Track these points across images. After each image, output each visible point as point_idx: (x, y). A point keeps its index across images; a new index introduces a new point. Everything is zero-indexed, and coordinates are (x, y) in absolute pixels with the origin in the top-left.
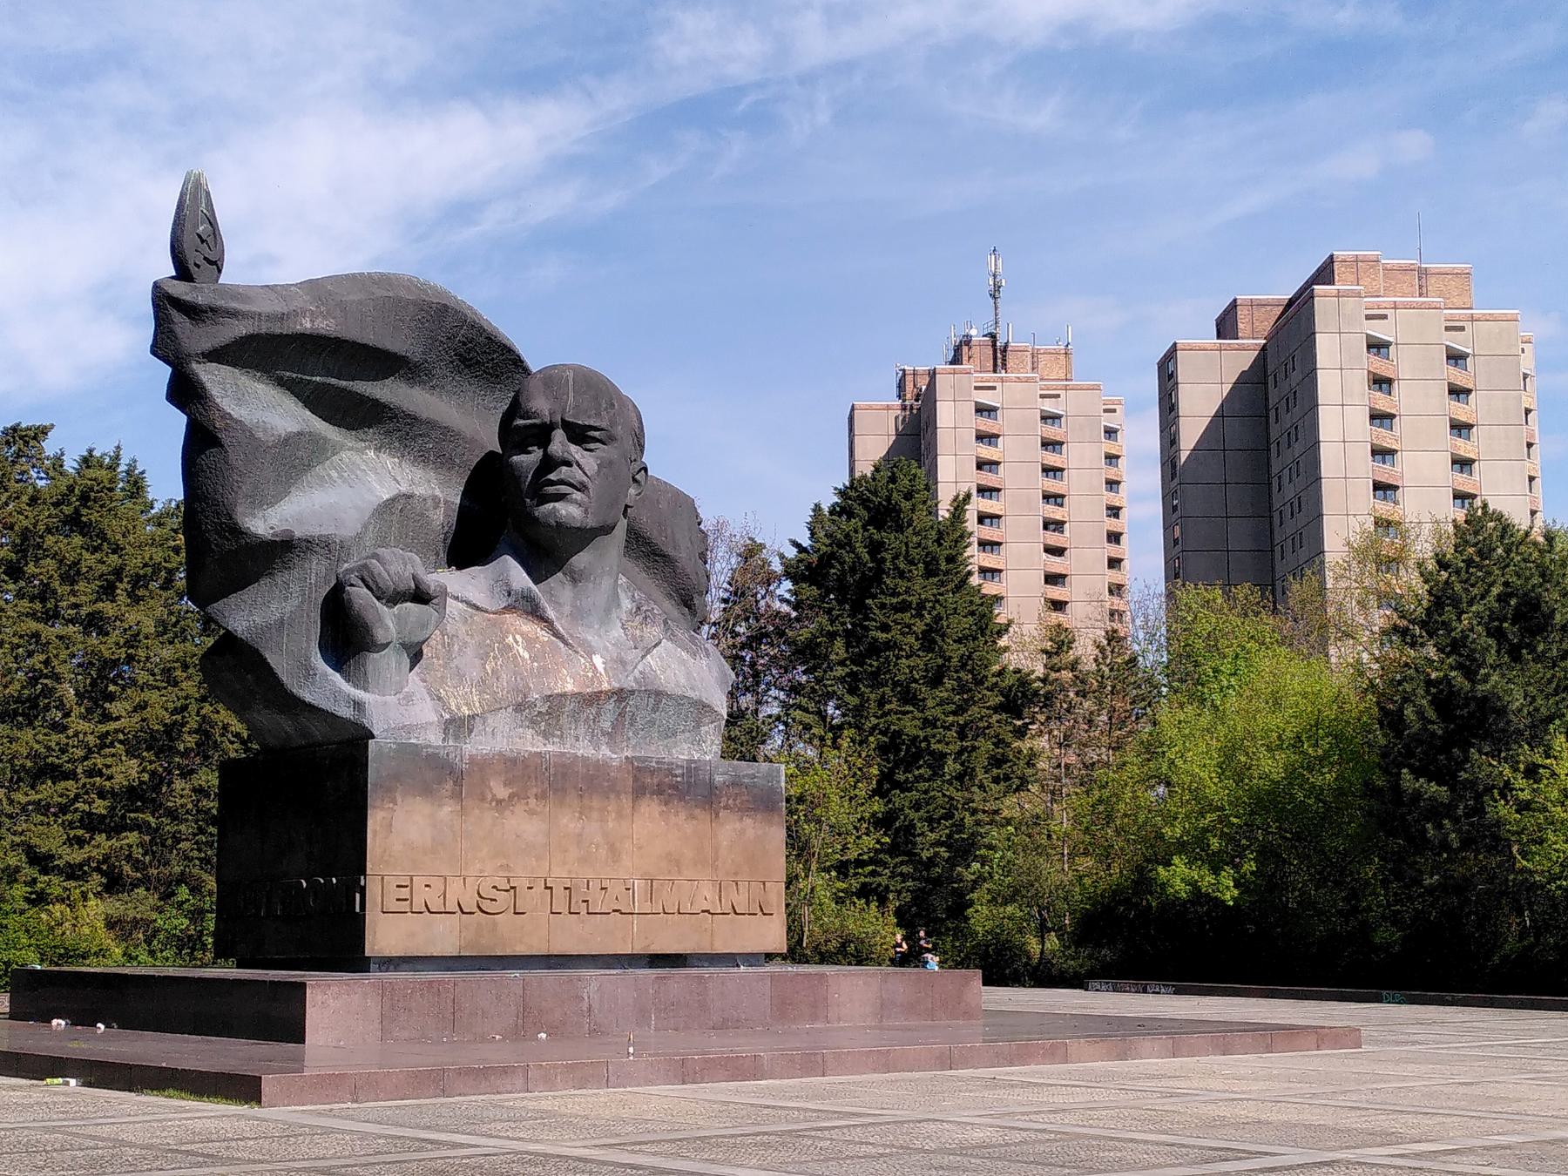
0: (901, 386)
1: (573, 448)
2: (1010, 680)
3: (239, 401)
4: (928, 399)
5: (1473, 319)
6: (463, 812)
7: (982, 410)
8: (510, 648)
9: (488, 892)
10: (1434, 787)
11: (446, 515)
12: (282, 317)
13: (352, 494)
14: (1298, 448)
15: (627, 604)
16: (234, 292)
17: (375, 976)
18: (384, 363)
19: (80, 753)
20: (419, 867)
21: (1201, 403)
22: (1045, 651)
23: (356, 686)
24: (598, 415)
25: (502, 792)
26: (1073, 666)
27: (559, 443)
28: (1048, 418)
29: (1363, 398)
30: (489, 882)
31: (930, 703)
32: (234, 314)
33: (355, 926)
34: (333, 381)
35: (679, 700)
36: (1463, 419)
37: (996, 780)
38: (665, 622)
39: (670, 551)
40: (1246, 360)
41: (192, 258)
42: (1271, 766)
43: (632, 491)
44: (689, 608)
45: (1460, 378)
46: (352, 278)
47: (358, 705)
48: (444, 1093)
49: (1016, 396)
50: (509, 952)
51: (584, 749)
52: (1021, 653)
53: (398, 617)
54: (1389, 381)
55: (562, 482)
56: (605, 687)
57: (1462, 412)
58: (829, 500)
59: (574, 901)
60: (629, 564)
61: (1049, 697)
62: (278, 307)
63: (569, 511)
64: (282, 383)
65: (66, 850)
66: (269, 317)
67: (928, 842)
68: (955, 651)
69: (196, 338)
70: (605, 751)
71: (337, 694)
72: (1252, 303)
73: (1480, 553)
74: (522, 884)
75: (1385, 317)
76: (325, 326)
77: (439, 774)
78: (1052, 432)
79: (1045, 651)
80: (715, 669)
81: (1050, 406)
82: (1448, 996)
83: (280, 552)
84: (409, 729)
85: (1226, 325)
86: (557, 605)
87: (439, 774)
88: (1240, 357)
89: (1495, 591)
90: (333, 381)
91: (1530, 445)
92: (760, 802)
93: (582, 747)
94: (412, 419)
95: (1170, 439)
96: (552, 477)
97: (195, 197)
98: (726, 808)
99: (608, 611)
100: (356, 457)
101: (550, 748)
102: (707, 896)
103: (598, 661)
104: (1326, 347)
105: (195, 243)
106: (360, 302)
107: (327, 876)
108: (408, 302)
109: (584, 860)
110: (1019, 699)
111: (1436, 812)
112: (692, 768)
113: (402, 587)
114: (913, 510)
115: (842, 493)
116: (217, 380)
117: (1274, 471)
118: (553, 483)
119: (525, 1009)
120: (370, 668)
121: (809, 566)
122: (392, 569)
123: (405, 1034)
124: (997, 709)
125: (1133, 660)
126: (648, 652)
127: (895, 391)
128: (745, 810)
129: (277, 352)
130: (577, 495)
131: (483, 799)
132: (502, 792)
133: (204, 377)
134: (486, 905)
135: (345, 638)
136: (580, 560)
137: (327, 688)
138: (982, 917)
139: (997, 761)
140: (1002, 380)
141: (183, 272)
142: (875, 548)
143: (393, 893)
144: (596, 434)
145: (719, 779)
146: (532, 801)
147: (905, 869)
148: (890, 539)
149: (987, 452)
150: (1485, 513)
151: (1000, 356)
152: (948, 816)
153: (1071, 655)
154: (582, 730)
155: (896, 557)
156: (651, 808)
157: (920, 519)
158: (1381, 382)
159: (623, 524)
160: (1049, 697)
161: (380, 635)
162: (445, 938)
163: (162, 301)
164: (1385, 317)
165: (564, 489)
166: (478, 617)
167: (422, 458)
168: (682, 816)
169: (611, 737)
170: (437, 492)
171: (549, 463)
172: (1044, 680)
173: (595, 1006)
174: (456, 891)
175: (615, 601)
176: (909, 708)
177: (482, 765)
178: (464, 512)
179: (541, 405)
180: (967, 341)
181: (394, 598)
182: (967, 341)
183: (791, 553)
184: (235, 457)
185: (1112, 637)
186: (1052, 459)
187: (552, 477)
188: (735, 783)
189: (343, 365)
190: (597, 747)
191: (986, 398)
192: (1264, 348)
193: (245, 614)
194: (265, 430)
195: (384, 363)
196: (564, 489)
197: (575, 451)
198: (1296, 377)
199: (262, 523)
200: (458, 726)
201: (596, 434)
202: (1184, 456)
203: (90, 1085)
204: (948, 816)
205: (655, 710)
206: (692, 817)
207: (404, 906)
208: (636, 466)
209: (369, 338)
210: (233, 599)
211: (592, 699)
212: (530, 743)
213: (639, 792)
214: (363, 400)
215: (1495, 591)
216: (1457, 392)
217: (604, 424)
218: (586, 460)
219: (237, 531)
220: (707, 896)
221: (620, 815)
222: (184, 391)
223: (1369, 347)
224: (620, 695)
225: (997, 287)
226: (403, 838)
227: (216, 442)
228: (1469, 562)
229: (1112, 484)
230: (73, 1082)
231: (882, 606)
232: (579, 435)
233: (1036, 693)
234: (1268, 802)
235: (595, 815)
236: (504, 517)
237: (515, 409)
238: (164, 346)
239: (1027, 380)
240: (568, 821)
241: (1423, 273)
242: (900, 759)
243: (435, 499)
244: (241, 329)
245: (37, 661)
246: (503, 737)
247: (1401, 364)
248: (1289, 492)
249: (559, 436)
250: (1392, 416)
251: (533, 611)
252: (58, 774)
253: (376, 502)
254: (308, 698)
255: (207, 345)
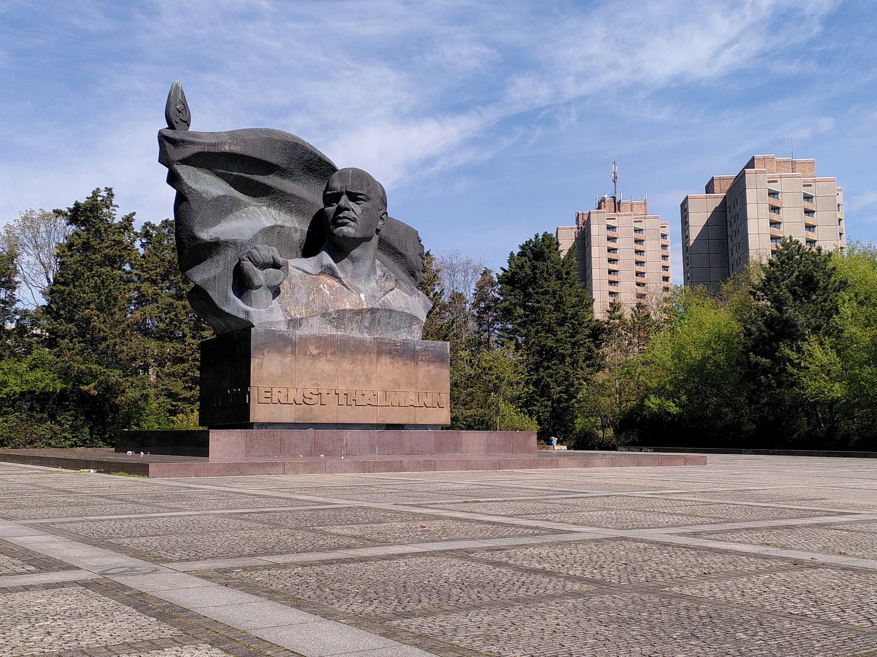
0: (577, 220)
1: (351, 203)
2: (593, 324)
3: (196, 182)
4: (587, 224)
5: (815, 181)
6: (296, 360)
7: (609, 228)
8: (321, 290)
9: (308, 395)
10: (764, 360)
11: (301, 236)
12: (215, 145)
13: (250, 222)
14: (739, 237)
15: (379, 273)
16: (194, 134)
17: (254, 431)
18: (269, 168)
19: (190, 352)
20: (274, 384)
21: (698, 220)
22: (608, 311)
23: (247, 305)
24: (362, 189)
25: (315, 352)
26: (620, 317)
27: (344, 201)
28: (637, 230)
29: (768, 215)
30: (309, 391)
31: (559, 333)
32: (192, 143)
33: (245, 409)
34: (243, 174)
35: (401, 314)
36: (811, 223)
37: (588, 366)
38: (396, 280)
39: (404, 252)
40: (717, 202)
41: (174, 119)
42: (697, 355)
43: (380, 223)
44: (414, 277)
45: (810, 206)
46: (252, 130)
47: (247, 313)
48: (242, 474)
49: (624, 222)
50: (318, 422)
51: (356, 334)
52: (599, 313)
53: (266, 275)
54: (778, 208)
55: (344, 217)
56: (365, 307)
57: (810, 220)
58: (517, 251)
59: (349, 400)
60: (379, 253)
61: (610, 330)
62: (213, 140)
63: (349, 230)
64: (218, 175)
65: (184, 391)
66: (209, 145)
67: (556, 391)
68: (570, 312)
69: (177, 154)
70: (366, 335)
71: (238, 308)
72: (720, 179)
73: (788, 258)
74: (324, 392)
75: (776, 181)
76: (236, 149)
77: (282, 343)
78: (639, 236)
79: (608, 311)
80: (422, 301)
81: (638, 225)
82: (771, 451)
83: (214, 247)
84: (271, 323)
85: (709, 188)
86: (343, 269)
87: (282, 343)
88: (715, 200)
89: (796, 273)
90: (243, 174)
91: (841, 234)
92: (438, 358)
93: (354, 333)
94: (283, 193)
95: (686, 237)
96: (341, 215)
97: (176, 91)
98: (422, 360)
99: (369, 275)
100: (256, 209)
101: (339, 333)
102: (412, 399)
103: (362, 296)
104: (751, 195)
105: (177, 114)
106: (253, 139)
107: (237, 389)
108: (278, 141)
109: (353, 382)
110: (597, 333)
111: (765, 371)
112: (405, 343)
113: (266, 261)
114: (550, 252)
115: (522, 247)
116: (184, 171)
117: (730, 248)
118: (341, 218)
119: (315, 444)
120: (253, 296)
121: (507, 278)
122: (262, 253)
123: (257, 454)
124: (589, 336)
125: (648, 316)
126: (387, 293)
127: (575, 222)
128: (430, 362)
129: (213, 160)
130: (352, 223)
131: (306, 355)
132: (315, 352)
133: (179, 171)
134: (307, 401)
135: (242, 284)
136: (356, 252)
137: (235, 306)
138: (579, 423)
139: (588, 358)
140: (618, 215)
141: (171, 126)
142: (534, 268)
143: (263, 395)
144: (361, 197)
145: (418, 348)
146: (329, 356)
147: (546, 403)
148: (539, 264)
149: (612, 245)
150: (791, 241)
151: (617, 206)
152: (566, 379)
153: (618, 313)
154: (355, 326)
155: (543, 272)
156: (385, 360)
157: (553, 256)
158: (775, 209)
159: (376, 238)
160: (610, 330)
161: (256, 282)
162: (288, 415)
163: (163, 138)
164: (776, 181)
165: (346, 221)
166: (308, 276)
167: (290, 211)
168: (401, 363)
169: (369, 329)
170: (297, 226)
171: (340, 210)
172: (608, 323)
173: (350, 443)
174: (292, 394)
175: (373, 269)
176: (549, 335)
177: (305, 340)
178: (309, 234)
179: (337, 185)
180: (603, 200)
181: (264, 266)
182: (603, 200)
183: (501, 273)
184: (194, 205)
185: (639, 306)
186: (639, 247)
187: (341, 215)
188: (426, 350)
189: (249, 168)
190: (362, 333)
191: (611, 223)
192: (725, 197)
193: (200, 275)
194: (207, 194)
195: (269, 168)
196: (346, 221)
197: (352, 204)
198: (738, 208)
199: (206, 235)
200: (294, 323)
201: (361, 197)
202: (691, 242)
203: (101, 472)
204: (566, 379)
205: (389, 318)
206: (405, 364)
207: (268, 400)
208: (382, 212)
209: (258, 155)
210: (195, 269)
211: (359, 312)
212: (329, 330)
213: (380, 353)
214: (259, 184)
215: (796, 273)
216: (808, 212)
217: (364, 192)
218: (356, 209)
219: (195, 238)
220: (412, 399)
221: (371, 362)
222: (173, 179)
223: (769, 194)
224: (373, 311)
225: (616, 178)
226: (265, 369)
227: (186, 200)
228: (783, 262)
229: (665, 257)
230: (92, 471)
231: (537, 293)
232: (353, 197)
233: (605, 329)
234: (697, 370)
235: (359, 362)
236: (323, 237)
237: (328, 188)
238: (164, 159)
239: (629, 215)
240: (346, 365)
241: (793, 163)
242: (546, 355)
243: (296, 230)
244: (196, 149)
245: (172, 315)
246: (316, 327)
247: (783, 201)
248: (736, 256)
249: (344, 198)
250: (780, 223)
251: (333, 274)
252: (182, 361)
253: (262, 227)
254: (227, 310)
255: (181, 157)
